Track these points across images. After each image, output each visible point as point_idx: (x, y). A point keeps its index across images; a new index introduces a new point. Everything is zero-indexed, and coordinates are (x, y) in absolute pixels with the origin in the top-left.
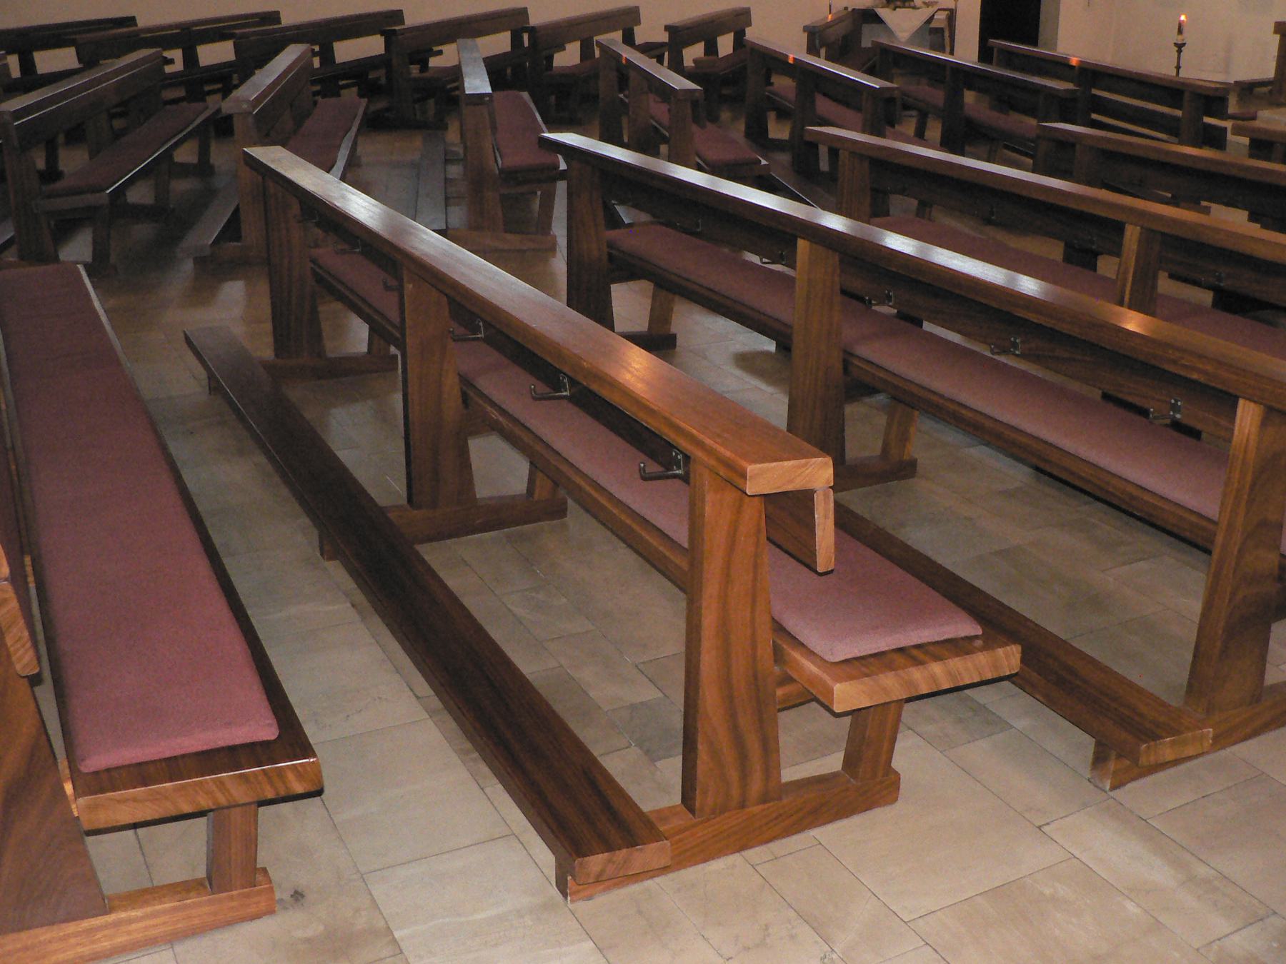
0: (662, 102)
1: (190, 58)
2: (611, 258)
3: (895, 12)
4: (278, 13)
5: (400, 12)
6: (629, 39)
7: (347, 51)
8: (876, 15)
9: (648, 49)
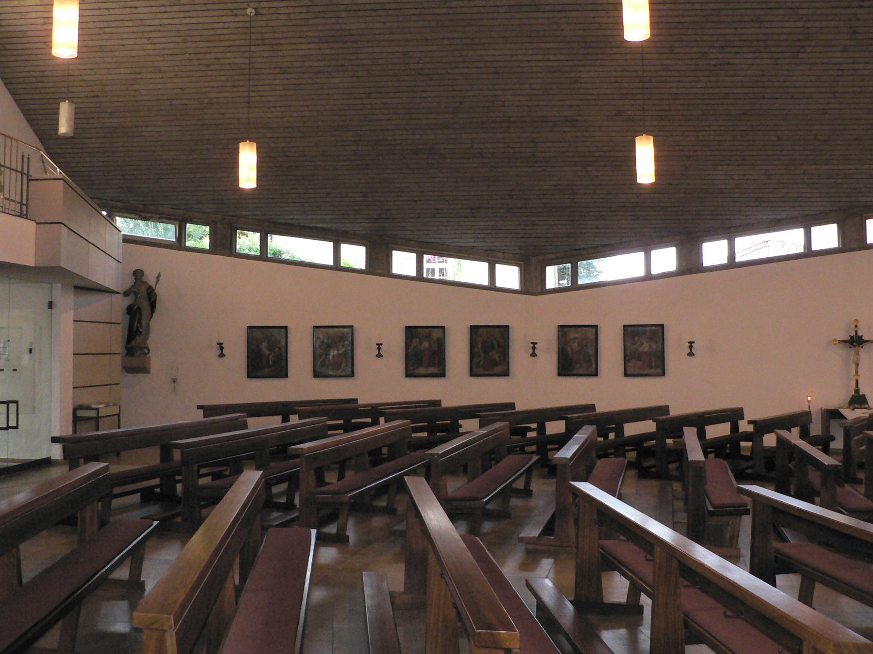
0: (817, 471)
1: (541, 429)
2: (603, 557)
3: (853, 412)
4: (440, 401)
5: (514, 404)
6: (804, 434)
7: (631, 429)
8: (840, 413)
9: (814, 442)
